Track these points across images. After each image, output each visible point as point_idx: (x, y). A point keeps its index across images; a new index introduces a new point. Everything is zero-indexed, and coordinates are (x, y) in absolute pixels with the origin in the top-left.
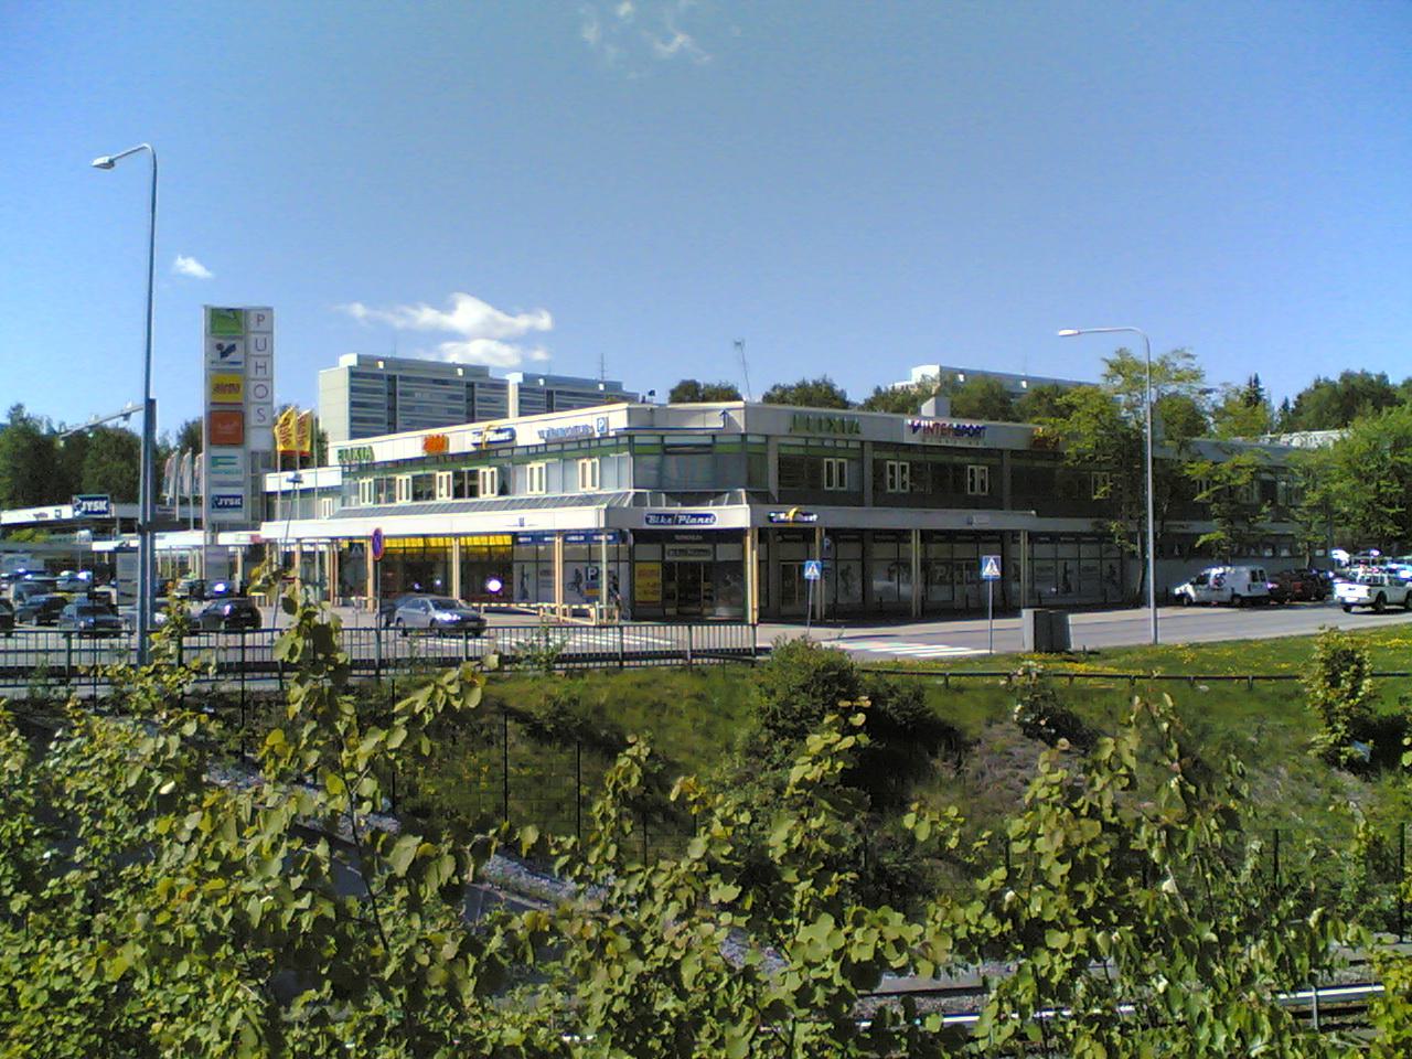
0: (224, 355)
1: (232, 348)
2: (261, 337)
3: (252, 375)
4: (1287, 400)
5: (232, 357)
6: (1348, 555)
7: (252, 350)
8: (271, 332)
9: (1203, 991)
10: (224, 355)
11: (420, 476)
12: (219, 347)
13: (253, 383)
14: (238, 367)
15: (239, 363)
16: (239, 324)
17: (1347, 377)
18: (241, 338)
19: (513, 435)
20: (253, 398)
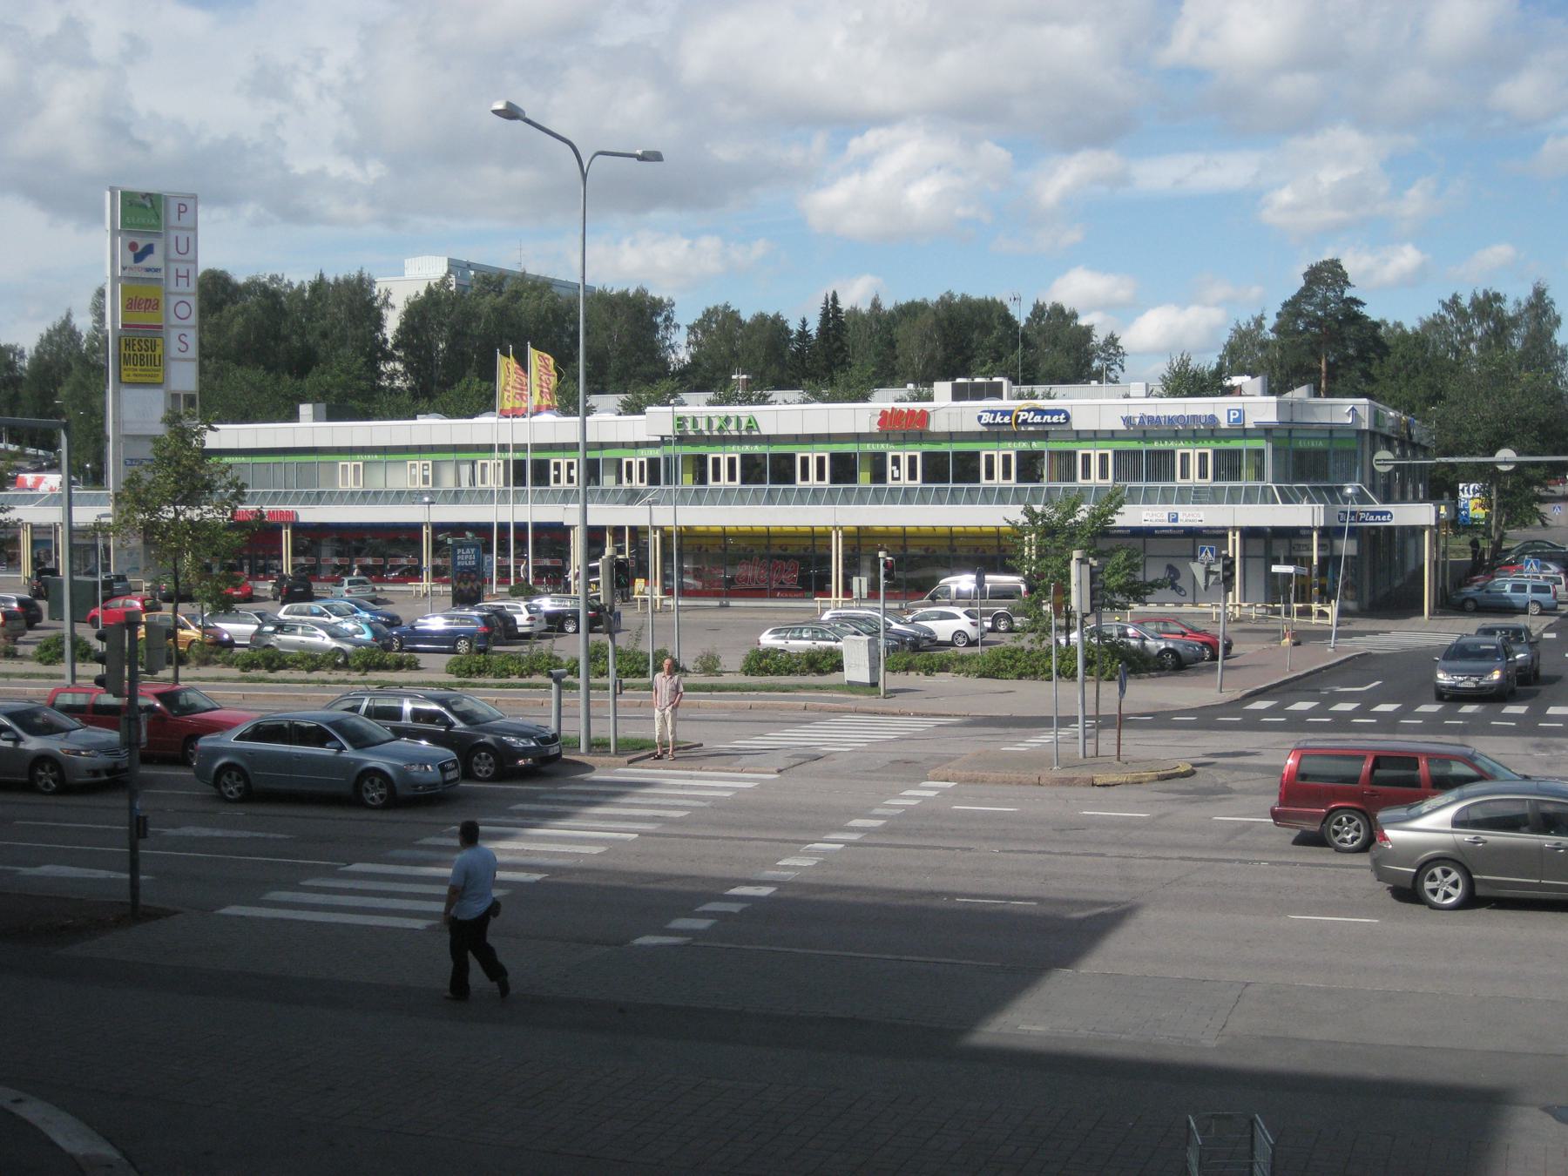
0: (139, 258)
1: (149, 250)
2: (183, 236)
3: (173, 288)
4: (1363, 304)
5: (149, 261)
6: (1320, 508)
7: (173, 254)
8: (195, 229)
9: (278, 379)
10: (139, 258)
11: (565, 554)
12: (133, 246)
13: (173, 300)
14: (155, 275)
15: (157, 270)
16: (158, 217)
17: (946, 303)
18: (158, 235)
19: (1068, 418)
20: (174, 320)
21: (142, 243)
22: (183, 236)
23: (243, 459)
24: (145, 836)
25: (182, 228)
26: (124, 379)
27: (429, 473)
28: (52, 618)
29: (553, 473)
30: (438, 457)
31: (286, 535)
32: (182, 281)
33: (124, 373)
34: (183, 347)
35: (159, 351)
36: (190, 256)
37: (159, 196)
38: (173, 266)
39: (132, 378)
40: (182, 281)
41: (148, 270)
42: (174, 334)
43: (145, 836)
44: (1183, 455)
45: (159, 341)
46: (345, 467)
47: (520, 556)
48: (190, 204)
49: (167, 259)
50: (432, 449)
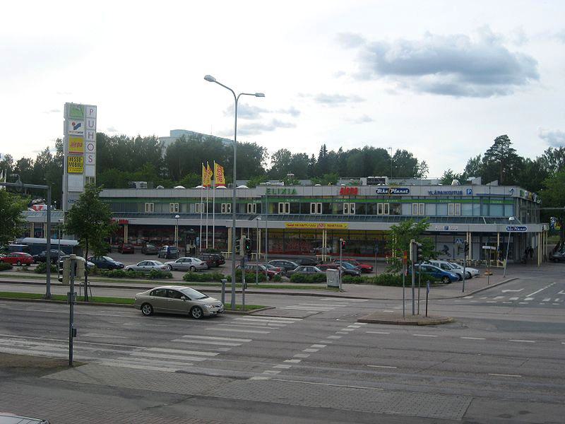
0: (75, 128)
1: (79, 125)
7: (88, 127)
49: (86, 129)
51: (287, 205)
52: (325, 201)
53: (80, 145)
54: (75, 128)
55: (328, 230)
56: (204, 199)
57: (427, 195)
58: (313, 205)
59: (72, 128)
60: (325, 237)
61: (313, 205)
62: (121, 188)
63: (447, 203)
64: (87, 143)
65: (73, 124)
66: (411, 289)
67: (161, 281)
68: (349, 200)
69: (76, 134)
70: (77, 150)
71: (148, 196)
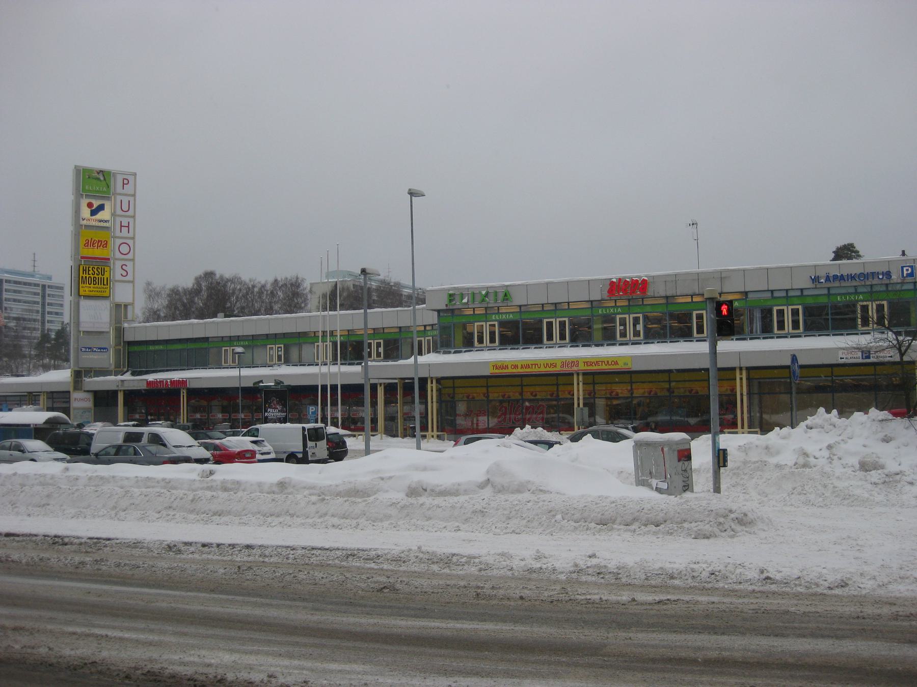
0: (93, 213)
1: (101, 208)
2: (125, 200)
5: (101, 215)
7: (119, 212)
18: (108, 198)
21: (96, 203)
22: (125, 200)
23: (161, 347)
24: (725, 466)
25: (126, 195)
26: (82, 293)
27: (282, 353)
28: (863, 326)
29: (381, 350)
30: (286, 341)
31: (184, 394)
32: (125, 230)
33: (81, 289)
34: (124, 273)
35: (107, 275)
36: (131, 213)
37: (109, 173)
38: (118, 220)
39: (87, 293)
40: (125, 230)
41: (100, 221)
42: (118, 264)
43: (725, 466)
44: (863, 307)
45: (107, 269)
46: (226, 351)
47: (334, 403)
48: (131, 179)
49: (114, 215)
50: (285, 335)
51: (562, 324)
52: (810, 301)
53: (104, 244)
54: (93, 213)
55: (585, 374)
56: (332, 333)
57: (808, 284)
58: (700, 317)
59: (86, 212)
60: (579, 391)
61: (550, 324)
62: (765, 351)
63: (266, 345)
64: (118, 242)
65: (90, 205)
66: (370, 326)
67: (186, 630)
68: (628, 309)
69: (94, 223)
70: (98, 252)
71: (191, 337)
